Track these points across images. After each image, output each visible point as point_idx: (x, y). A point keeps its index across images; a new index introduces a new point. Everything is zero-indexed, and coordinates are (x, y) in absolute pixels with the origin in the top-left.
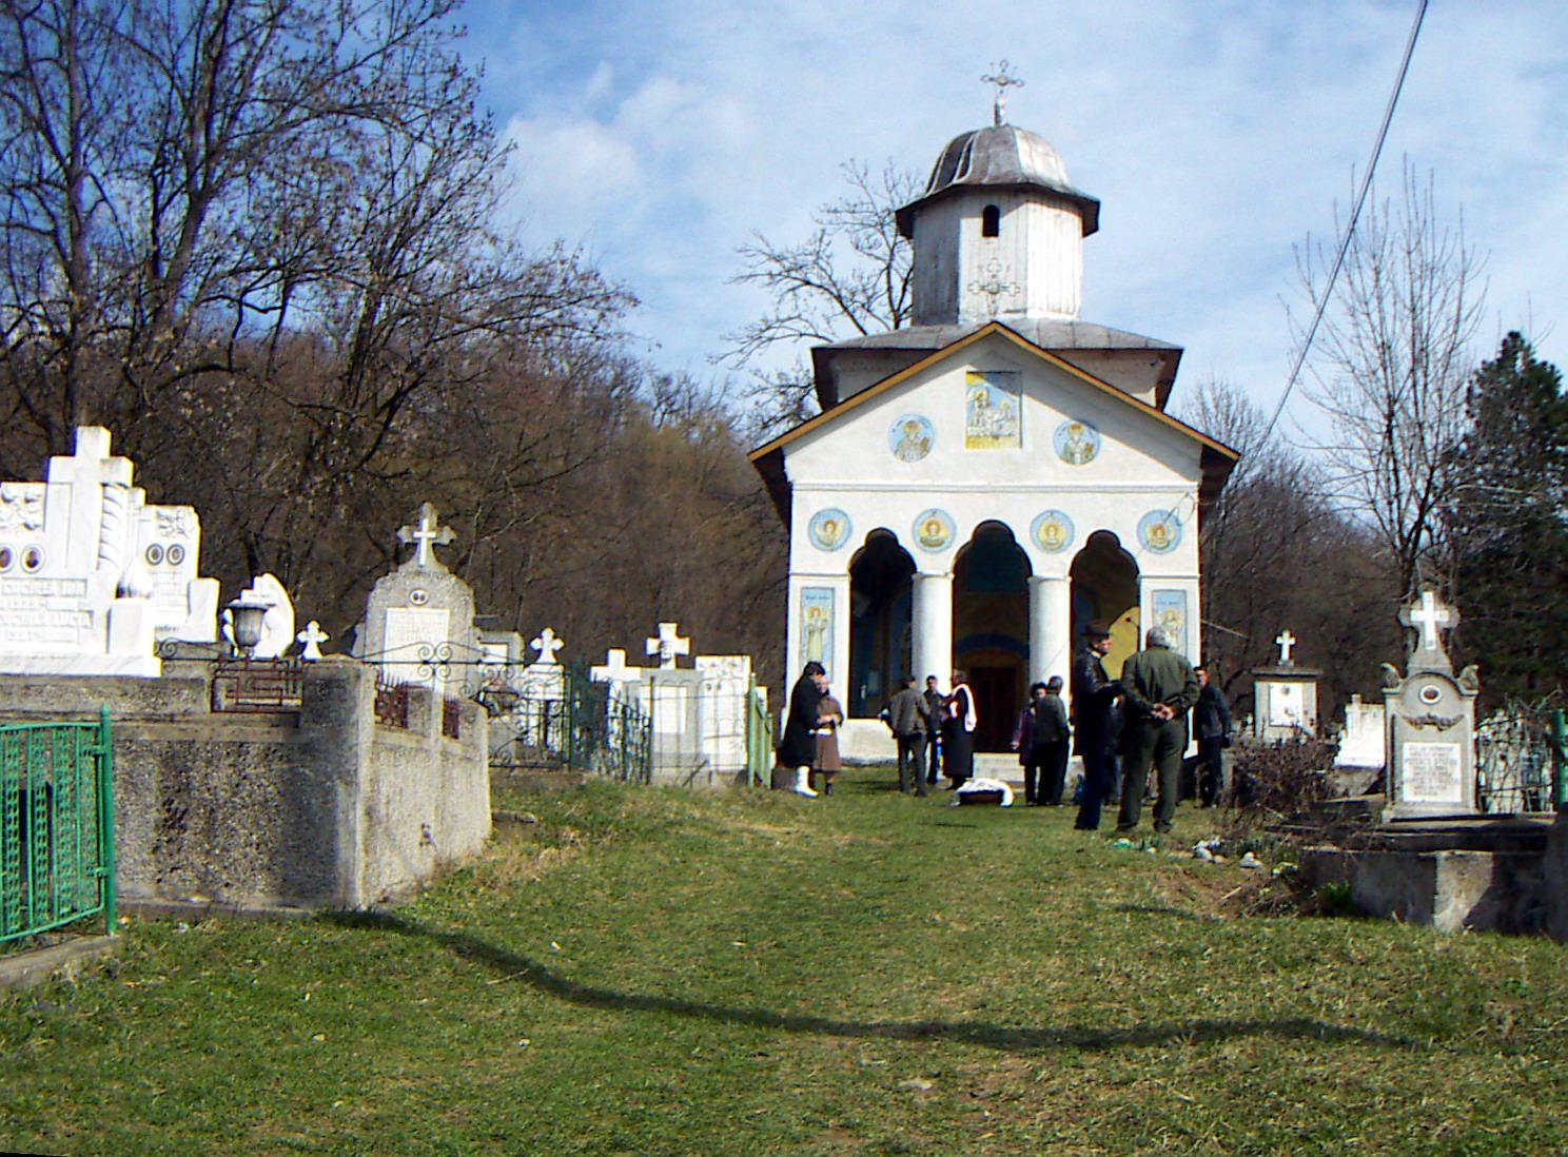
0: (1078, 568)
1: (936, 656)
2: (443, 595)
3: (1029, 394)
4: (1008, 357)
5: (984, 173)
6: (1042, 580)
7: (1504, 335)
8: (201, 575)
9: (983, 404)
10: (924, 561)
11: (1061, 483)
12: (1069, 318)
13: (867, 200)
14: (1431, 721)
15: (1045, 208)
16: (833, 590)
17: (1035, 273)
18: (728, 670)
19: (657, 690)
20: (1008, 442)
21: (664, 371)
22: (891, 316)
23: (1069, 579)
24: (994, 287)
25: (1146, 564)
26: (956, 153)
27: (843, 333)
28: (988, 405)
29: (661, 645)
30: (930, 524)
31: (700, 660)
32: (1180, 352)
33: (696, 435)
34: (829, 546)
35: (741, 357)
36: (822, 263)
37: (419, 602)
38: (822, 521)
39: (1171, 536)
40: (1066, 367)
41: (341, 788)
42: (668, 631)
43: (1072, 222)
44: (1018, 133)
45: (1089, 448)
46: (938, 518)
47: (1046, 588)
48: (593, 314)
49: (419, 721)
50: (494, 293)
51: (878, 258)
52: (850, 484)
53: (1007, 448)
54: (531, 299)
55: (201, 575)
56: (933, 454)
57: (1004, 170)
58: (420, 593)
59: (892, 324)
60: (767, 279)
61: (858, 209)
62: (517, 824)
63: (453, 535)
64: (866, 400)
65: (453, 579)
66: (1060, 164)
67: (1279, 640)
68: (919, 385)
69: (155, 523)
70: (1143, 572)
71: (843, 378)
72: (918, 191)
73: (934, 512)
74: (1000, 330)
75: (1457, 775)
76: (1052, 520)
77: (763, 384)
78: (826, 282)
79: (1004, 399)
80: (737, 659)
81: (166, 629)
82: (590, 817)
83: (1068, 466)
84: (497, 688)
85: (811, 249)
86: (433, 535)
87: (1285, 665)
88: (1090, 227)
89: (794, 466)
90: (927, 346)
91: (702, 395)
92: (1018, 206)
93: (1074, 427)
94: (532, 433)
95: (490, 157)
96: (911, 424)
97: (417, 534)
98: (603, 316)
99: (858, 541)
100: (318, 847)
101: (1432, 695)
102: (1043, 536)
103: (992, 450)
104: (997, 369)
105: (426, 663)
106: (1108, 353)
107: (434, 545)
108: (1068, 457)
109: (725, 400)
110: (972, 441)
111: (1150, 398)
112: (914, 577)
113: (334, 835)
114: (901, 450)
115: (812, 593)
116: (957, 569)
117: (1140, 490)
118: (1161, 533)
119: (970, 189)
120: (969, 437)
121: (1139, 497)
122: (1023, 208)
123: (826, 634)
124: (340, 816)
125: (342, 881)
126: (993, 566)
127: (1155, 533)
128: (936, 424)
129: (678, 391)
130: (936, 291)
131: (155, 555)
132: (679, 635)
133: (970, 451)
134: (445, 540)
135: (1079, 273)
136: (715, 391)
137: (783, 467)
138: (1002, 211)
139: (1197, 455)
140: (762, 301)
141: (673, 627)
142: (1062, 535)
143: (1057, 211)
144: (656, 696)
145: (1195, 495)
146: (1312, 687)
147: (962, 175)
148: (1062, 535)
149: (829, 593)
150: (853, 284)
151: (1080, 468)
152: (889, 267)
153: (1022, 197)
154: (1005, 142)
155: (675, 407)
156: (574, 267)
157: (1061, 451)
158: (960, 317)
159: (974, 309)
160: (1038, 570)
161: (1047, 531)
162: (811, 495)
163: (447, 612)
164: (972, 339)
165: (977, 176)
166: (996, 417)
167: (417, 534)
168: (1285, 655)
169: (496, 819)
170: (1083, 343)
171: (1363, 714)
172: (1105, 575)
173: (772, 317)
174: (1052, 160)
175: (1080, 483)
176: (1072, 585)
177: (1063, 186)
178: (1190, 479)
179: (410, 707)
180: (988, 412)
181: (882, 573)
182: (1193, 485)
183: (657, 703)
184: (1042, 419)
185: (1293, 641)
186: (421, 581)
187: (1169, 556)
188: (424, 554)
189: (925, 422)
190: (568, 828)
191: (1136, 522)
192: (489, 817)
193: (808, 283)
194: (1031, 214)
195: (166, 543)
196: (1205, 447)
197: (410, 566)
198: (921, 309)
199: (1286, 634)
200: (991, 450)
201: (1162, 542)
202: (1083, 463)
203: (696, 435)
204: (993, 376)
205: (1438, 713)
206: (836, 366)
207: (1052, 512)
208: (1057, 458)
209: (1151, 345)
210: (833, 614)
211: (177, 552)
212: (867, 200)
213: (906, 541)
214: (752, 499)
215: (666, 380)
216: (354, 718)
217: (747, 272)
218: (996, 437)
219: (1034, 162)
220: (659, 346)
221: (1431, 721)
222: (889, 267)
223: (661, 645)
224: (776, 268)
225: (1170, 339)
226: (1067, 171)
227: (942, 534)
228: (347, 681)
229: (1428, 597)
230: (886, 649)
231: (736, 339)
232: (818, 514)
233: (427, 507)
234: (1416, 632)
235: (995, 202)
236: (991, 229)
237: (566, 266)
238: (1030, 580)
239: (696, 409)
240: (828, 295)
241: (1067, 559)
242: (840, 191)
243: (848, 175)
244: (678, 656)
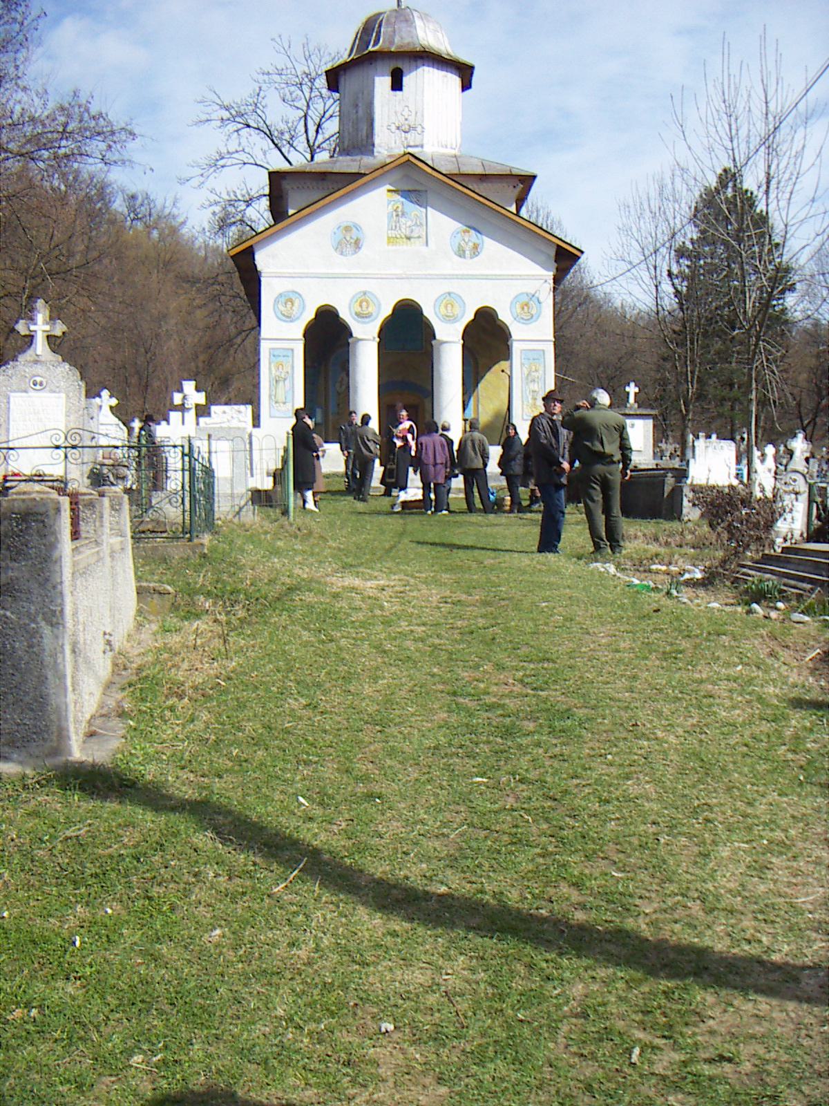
0: (468, 333)
1: (366, 398)
2: (58, 381)
3: (432, 207)
4: (416, 178)
5: (392, 43)
6: (443, 343)
7: (719, 171)
9: (399, 214)
10: (357, 329)
11: (456, 272)
12: (453, 152)
13: (290, 65)
15: (435, 70)
16: (292, 350)
17: (426, 117)
18: (235, 416)
19: (213, 442)
20: (417, 241)
21: (132, 189)
22: (308, 150)
23: (462, 342)
25: (517, 331)
26: (370, 28)
27: (280, 165)
28: (403, 214)
29: (184, 398)
30: (361, 303)
31: (213, 408)
32: (534, 177)
33: (155, 234)
34: (289, 318)
35: (202, 179)
36: (258, 111)
37: (38, 387)
38: (283, 299)
39: (533, 312)
40: (460, 188)
41: (46, 630)
42: (189, 386)
43: (454, 81)
44: (415, 14)
45: (476, 247)
47: (445, 348)
48: (103, 146)
49: (91, 528)
50: (28, 129)
51: (298, 108)
52: (304, 272)
53: (417, 245)
54: (78, 126)
57: (406, 41)
58: (38, 379)
59: (309, 156)
60: (219, 123)
61: (284, 72)
62: (156, 596)
63: (65, 328)
64: (310, 211)
65: (67, 366)
66: (446, 38)
68: (352, 200)
70: (514, 337)
71: (291, 195)
72: (344, 57)
76: (450, 298)
77: (217, 199)
78: (261, 125)
79: (414, 210)
80: (242, 408)
82: (219, 586)
84: (111, 462)
85: (251, 101)
86: (47, 328)
87: (631, 408)
88: (466, 86)
89: (263, 259)
90: (353, 171)
91: (159, 207)
92: (417, 67)
93: (464, 232)
94: (58, 236)
95: (26, 23)
96: (348, 229)
97: (32, 328)
98: (110, 147)
99: (310, 315)
100: (26, 693)
102: (443, 310)
103: (406, 247)
104: (410, 188)
105: (57, 447)
106: (483, 178)
107: (48, 337)
108: (461, 253)
109: (175, 211)
110: (391, 240)
111: (513, 209)
112: (350, 340)
113: (42, 680)
114: (340, 247)
115: (276, 353)
116: (381, 333)
118: (527, 306)
119: (379, 56)
120: (389, 238)
121: (514, 285)
122: (420, 70)
123: (287, 382)
124: (48, 660)
125: (54, 729)
126: (407, 331)
127: (523, 309)
129: (142, 205)
132: (198, 389)
134: (58, 332)
135: (459, 119)
136: (167, 205)
137: (254, 259)
138: (404, 70)
139: (553, 253)
140: (215, 139)
141: (193, 383)
143: (444, 73)
144: (213, 449)
146: (650, 422)
147: (374, 46)
148: (457, 311)
149: (290, 353)
150: (283, 127)
151: (470, 261)
152: (305, 116)
153: (419, 62)
154: (407, 21)
155: (140, 216)
156: (87, 110)
157: (456, 249)
158: (375, 150)
159: (387, 144)
160: (440, 335)
161: (446, 307)
163: (63, 395)
164: (392, 165)
165: (387, 45)
166: (409, 223)
167: (32, 328)
168: (632, 399)
169: (140, 592)
170: (465, 170)
171: (707, 447)
172: (487, 339)
173: (224, 150)
174: (440, 35)
175: (470, 272)
176: (463, 346)
177: (448, 55)
178: (547, 269)
179: (81, 514)
180: (403, 220)
181: (327, 338)
182: (550, 275)
183: (213, 455)
184: (442, 226)
185: (637, 390)
186: (39, 369)
188: (40, 346)
189: (357, 227)
190: (202, 598)
191: (510, 299)
192: (134, 588)
193: (248, 126)
194: (426, 75)
196: (558, 246)
197: (28, 355)
198: (346, 143)
200: (405, 247)
203: (155, 234)
204: (407, 194)
206: (286, 185)
207: (449, 294)
208: (453, 254)
209: (515, 172)
210: (293, 367)
212: (290, 65)
213: (345, 314)
214: (210, 281)
215: (133, 197)
216: (56, 555)
217: (204, 117)
219: (428, 35)
220: (152, 170)
222: (305, 116)
223: (184, 398)
224: (226, 115)
225: (522, 166)
226: (450, 44)
227: (370, 309)
228: (46, 514)
230: (326, 389)
231: (199, 166)
232: (281, 295)
233: (40, 303)
235: (400, 66)
236: (397, 85)
237: (82, 110)
238: (433, 342)
239: (155, 216)
240: (263, 135)
242: (272, 59)
243: (277, 46)
244: (197, 406)
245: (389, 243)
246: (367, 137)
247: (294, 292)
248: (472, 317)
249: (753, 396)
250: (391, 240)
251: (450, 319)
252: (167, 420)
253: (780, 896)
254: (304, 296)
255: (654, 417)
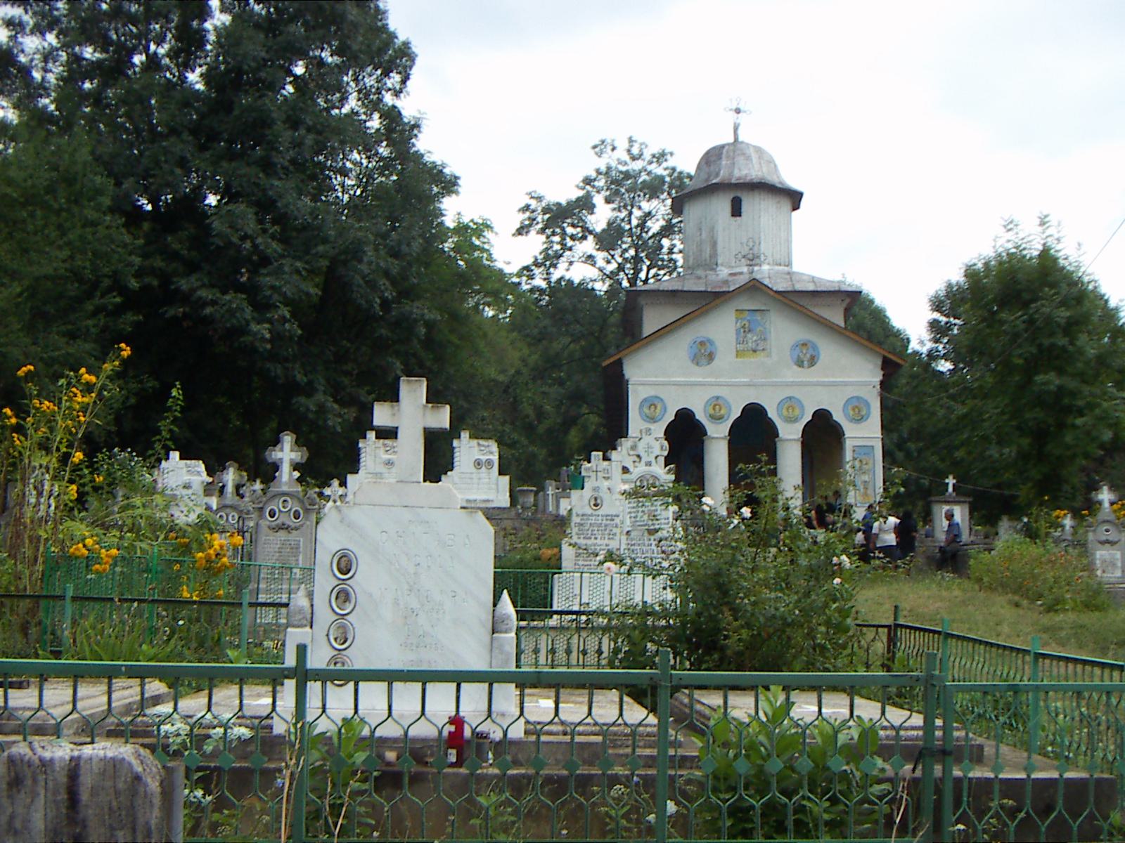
6: (782, 440)
8: (500, 474)
14: (1107, 542)
24: (750, 256)
30: (715, 405)
34: (653, 420)
38: (647, 404)
46: (720, 402)
53: (761, 357)
55: (500, 474)
56: (716, 362)
67: (947, 481)
69: (477, 449)
73: (718, 398)
74: (757, 284)
75: (1119, 564)
76: (790, 403)
81: (488, 501)
83: (800, 369)
96: (702, 343)
101: (1107, 531)
102: (785, 413)
106: (815, 294)
108: (800, 364)
110: (739, 354)
114: (696, 360)
117: (846, 384)
126: (753, 432)
128: (717, 343)
130: (701, 251)
131: (479, 464)
133: (739, 360)
139: (879, 362)
142: (797, 412)
145: (879, 387)
148: (797, 412)
161: (788, 409)
162: (640, 388)
166: (755, 338)
168: (950, 489)
170: (799, 287)
172: (822, 435)
180: (749, 335)
187: (863, 425)
189: (711, 342)
195: (484, 458)
199: (951, 477)
201: (859, 417)
202: (809, 367)
205: (1110, 539)
207: (790, 398)
209: (844, 288)
211: (489, 462)
213: (700, 416)
218: (755, 351)
221: (1107, 542)
227: (722, 412)
229: (1105, 488)
234: (1100, 503)
235: (739, 194)
236: (736, 211)
241: (800, 426)
245: (737, 356)
246: (710, 257)
247: (657, 397)
248: (810, 418)
249: (1039, 392)
250: (739, 354)
251: (791, 420)
252: (459, 437)
253: (540, 341)
254: (666, 401)
255: (970, 503)
